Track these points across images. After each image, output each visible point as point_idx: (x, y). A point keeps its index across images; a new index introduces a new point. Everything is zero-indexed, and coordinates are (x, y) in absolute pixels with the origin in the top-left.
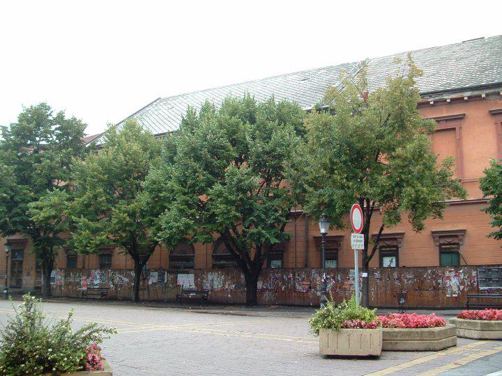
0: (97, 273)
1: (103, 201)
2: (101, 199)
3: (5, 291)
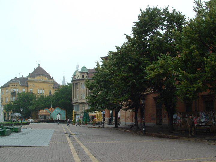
0: (203, 114)
1: (196, 55)
2: (194, 54)
3: (144, 129)
